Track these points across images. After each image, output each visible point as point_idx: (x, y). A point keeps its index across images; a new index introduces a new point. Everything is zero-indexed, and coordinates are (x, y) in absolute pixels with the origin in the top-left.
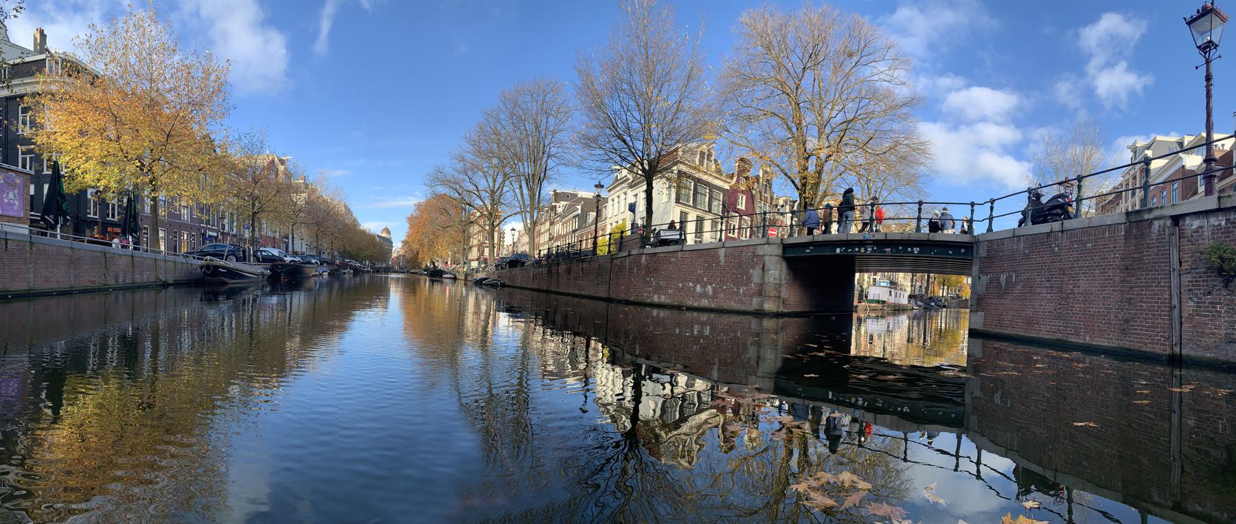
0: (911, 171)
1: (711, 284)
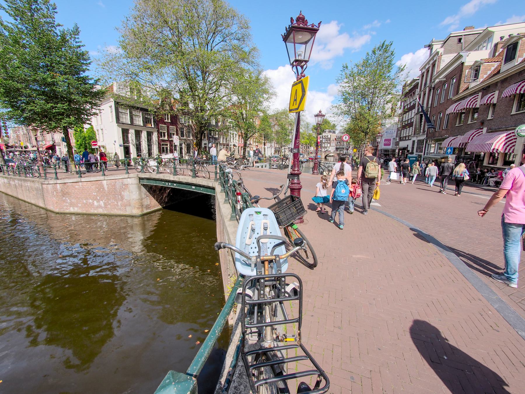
1: (102, 200)
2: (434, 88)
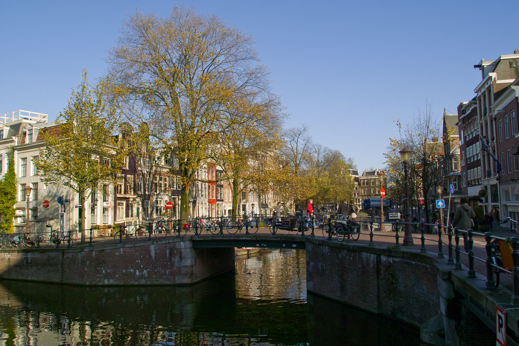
0: (249, 47)
1: (146, 269)
2: (495, 119)
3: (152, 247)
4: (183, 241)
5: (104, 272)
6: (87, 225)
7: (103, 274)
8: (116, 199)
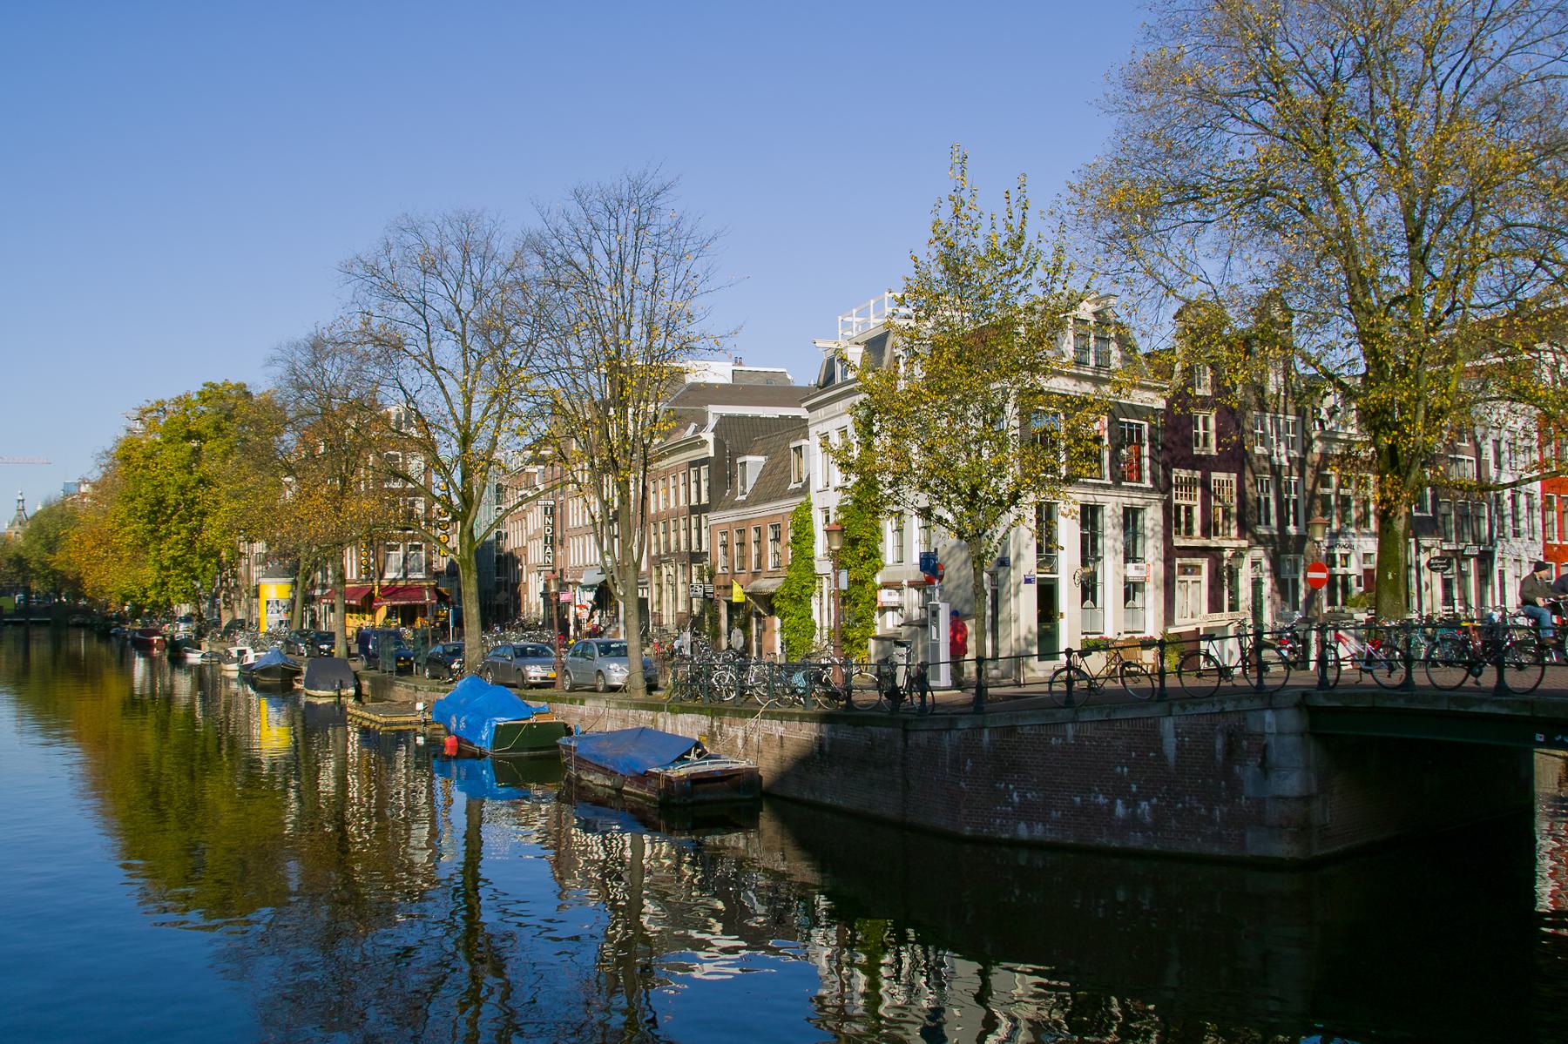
1: (1148, 799)
3: (1168, 725)
4: (1274, 709)
5: (1016, 799)
6: (1068, 635)
7: (1012, 804)
8: (1170, 553)
